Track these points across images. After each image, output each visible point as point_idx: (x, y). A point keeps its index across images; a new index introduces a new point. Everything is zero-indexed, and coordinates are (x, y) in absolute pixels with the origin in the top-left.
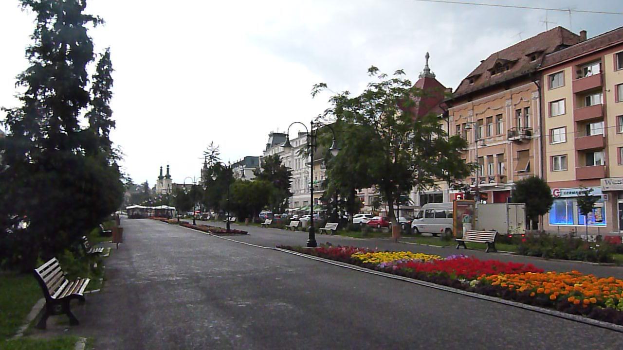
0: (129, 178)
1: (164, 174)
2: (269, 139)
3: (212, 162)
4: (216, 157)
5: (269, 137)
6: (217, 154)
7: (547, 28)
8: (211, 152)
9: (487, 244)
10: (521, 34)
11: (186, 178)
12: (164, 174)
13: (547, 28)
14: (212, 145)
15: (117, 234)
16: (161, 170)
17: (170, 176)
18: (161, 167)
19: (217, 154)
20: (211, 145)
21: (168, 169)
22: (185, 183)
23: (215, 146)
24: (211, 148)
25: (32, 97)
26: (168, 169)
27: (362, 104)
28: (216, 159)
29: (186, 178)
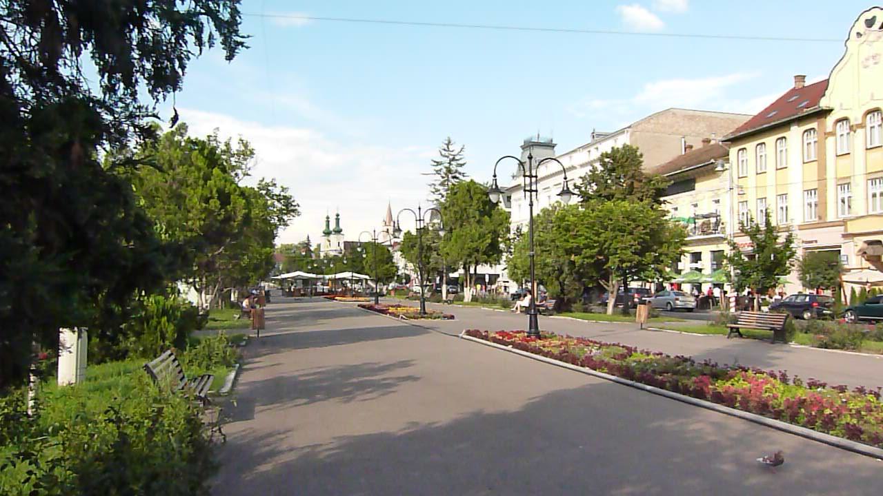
0: (285, 197)
1: (332, 226)
2: (522, 153)
3: (448, 180)
4: (456, 171)
5: (522, 151)
6: (461, 165)
7: (847, 282)
8: (447, 160)
9: (773, 332)
10: (758, 189)
11: (361, 233)
12: (332, 226)
13: (847, 282)
14: (448, 145)
15: (43, 428)
16: (328, 222)
17: (341, 231)
18: (338, 215)
19: (461, 165)
20: (445, 147)
21: (338, 220)
22: (361, 241)
23: (455, 148)
24: (447, 153)
25: (40, 34)
26: (338, 220)
27: (16, 438)
28: (457, 175)
29: (361, 233)
